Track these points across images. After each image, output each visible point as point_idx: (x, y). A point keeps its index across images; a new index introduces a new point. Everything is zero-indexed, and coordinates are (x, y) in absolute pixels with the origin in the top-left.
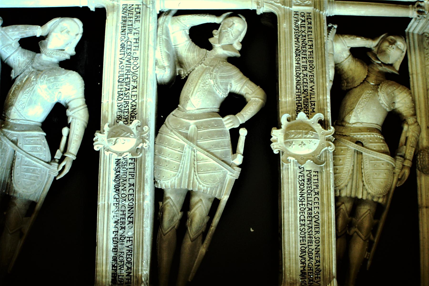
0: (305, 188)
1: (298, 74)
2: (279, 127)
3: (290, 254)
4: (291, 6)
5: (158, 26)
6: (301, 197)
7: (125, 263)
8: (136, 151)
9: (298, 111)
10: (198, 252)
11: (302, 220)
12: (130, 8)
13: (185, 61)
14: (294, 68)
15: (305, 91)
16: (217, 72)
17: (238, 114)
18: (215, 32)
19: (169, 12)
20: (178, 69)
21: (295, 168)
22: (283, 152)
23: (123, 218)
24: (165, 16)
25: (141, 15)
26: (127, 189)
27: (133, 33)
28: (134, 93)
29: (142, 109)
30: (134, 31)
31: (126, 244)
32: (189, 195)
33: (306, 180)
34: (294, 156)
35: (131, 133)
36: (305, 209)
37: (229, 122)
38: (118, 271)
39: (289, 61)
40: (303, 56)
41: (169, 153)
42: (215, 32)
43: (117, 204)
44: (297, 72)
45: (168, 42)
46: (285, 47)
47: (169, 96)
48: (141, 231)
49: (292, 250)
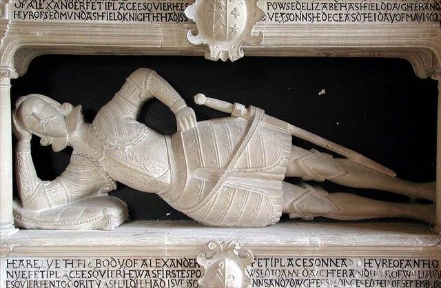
0: (294, 12)
1: (120, 17)
2: (206, 47)
3: (389, 37)
4: (6, 22)
5: (38, 229)
6: (306, 19)
7: (401, 269)
8: (242, 256)
9: (182, 18)
10: (360, 164)
11: (340, 18)
12: (12, 277)
13: (91, 186)
14: (109, 22)
15: (146, 8)
16: (112, 140)
17: (173, 109)
18: (44, 143)
19: (15, 213)
20: (99, 194)
21: (265, 26)
22: (244, 43)
23: (338, 273)
24: (23, 218)
25: (25, 259)
26: (296, 268)
27: (57, 269)
28: (154, 264)
29: (180, 251)
30: (53, 268)
31: (375, 268)
32: (291, 180)
33: (282, 11)
34: (249, 26)
35: (216, 266)
36: (324, 14)
37: (187, 121)
38: (413, 278)
39: (98, 29)
40: (90, 7)
41: (238, 207)
42: (44, 143)
43: (317, 283)
44: (116, 18)
45: (64, 213)
46: (75, 35)
47: (142, 207)
48: (361, 248)
49: (384, 32)
